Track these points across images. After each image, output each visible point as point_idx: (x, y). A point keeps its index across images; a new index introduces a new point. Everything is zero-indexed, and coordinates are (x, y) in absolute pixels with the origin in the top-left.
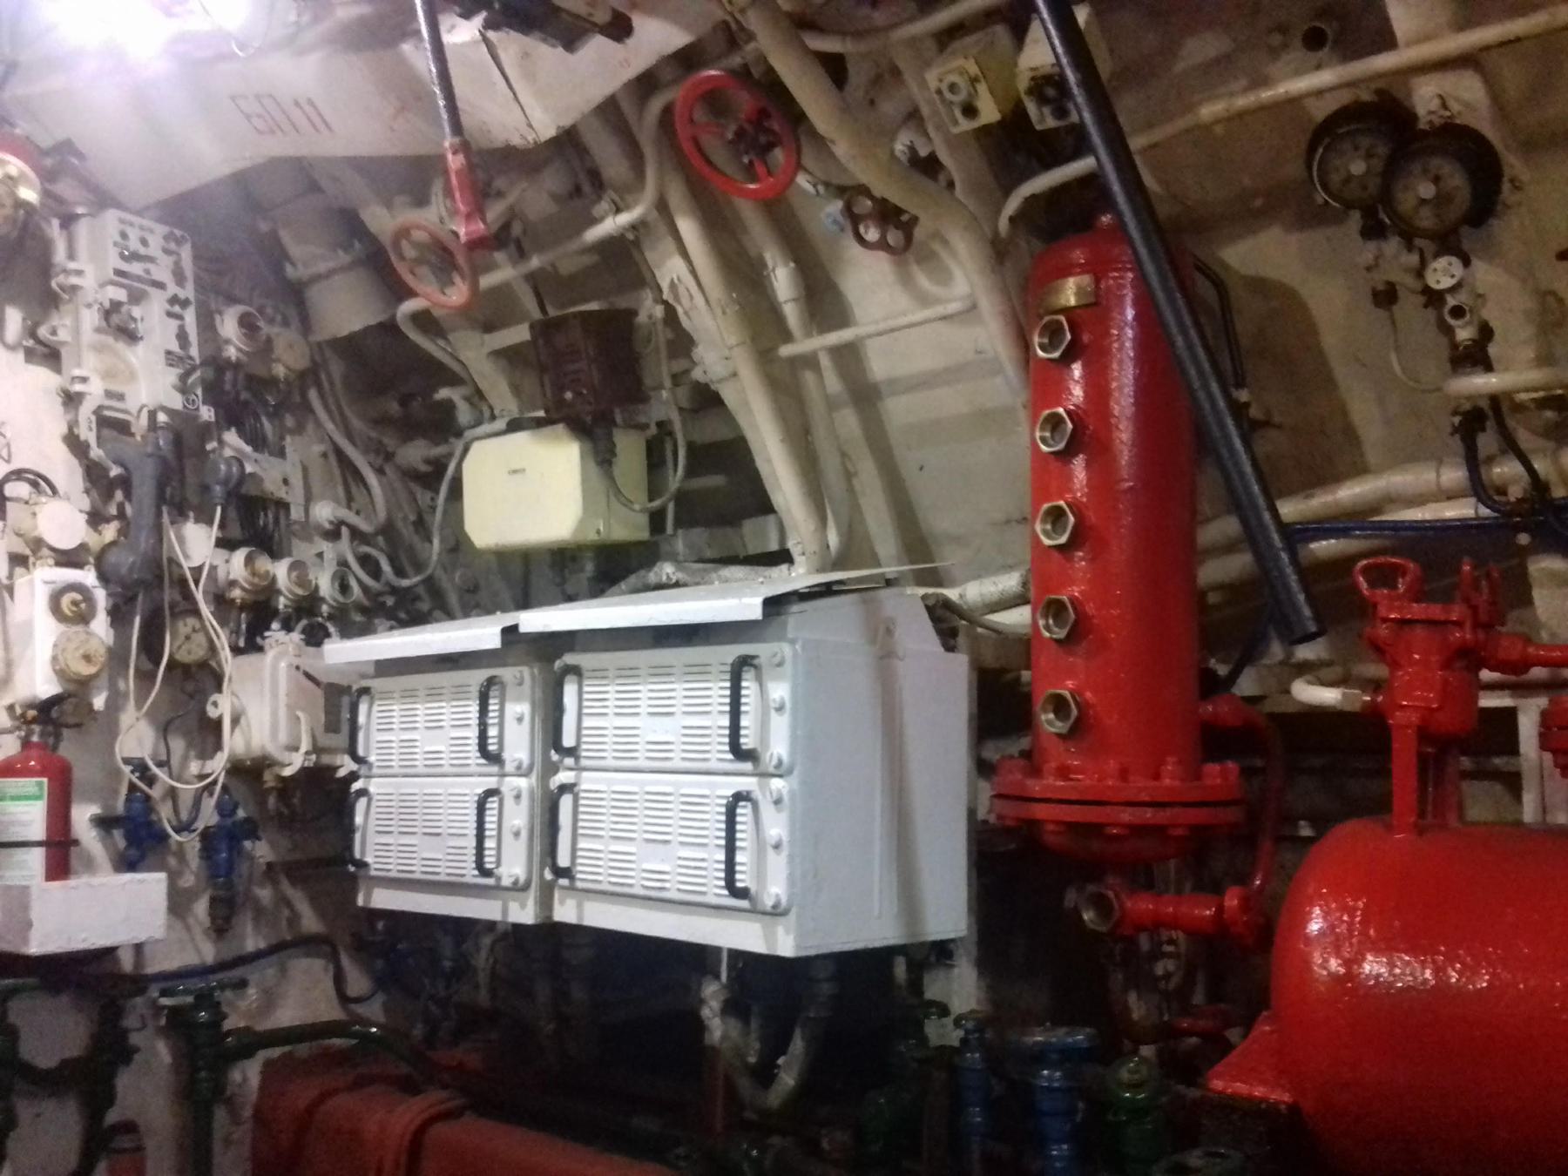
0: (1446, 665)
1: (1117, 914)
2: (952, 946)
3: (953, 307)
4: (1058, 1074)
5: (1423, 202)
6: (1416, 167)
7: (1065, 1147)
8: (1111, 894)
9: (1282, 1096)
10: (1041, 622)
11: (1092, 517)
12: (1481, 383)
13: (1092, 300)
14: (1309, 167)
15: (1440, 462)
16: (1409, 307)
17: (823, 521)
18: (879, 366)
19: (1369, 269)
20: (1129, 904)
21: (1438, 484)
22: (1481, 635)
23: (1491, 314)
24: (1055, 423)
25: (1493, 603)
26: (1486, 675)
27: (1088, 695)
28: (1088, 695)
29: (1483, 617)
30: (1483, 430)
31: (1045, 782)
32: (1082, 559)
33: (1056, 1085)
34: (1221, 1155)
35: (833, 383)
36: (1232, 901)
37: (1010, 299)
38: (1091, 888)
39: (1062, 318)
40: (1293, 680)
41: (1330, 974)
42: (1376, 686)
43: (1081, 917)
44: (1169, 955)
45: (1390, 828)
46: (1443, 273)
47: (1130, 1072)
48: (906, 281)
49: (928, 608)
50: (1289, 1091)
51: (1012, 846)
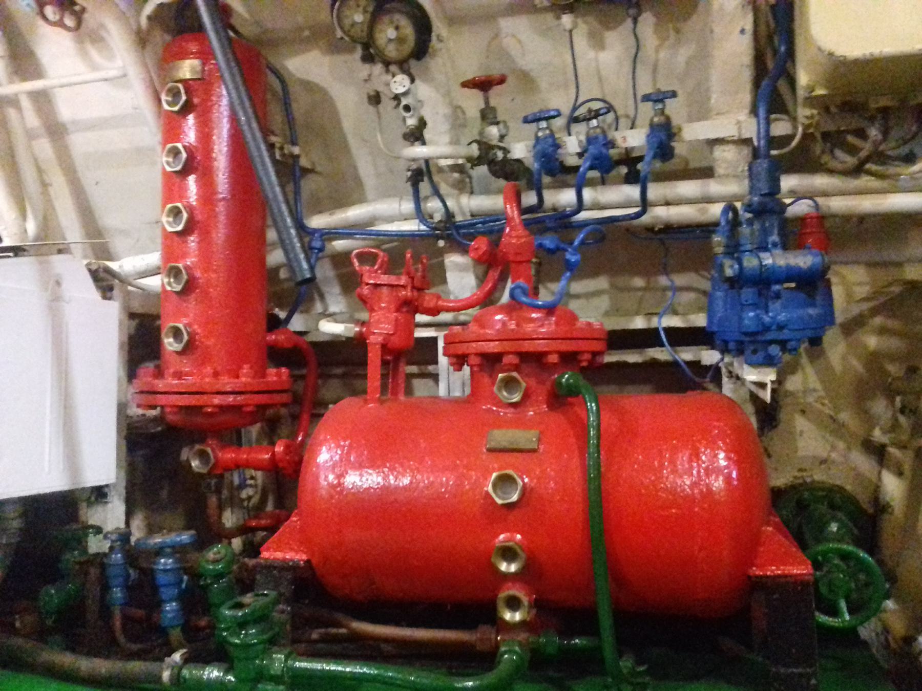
0: (398, 310)
1: (213, 460)
2: (106, 490)
3: (112, 73)
4: (171, 560)
5: (390, 40)
6: (386, 19)
7: (174, 604)
8: (209, 450)
9: (299, 557)
10: (166, 280)
11: (199, 217)
12: (419, 151)
13: (199, 76)
14: (332, 11)
15: (401, 199)
16: (387, 104)
17: (24, 216)
18: (66, 111)
19: (366, 81)
20: (220, 454)
21: (400, 210)
22: (416, 293)
23: (426, 113)
24: (175, 153)
25: (424, 277)
26: (420, 318)
27: (196, 327)
28: (196, 327)
29: (417, 283)
30: (422, 181)
31: (166, 381)
32: (193, 241)
33: (169, 567)
34: (266, 595)
35: (32, 120)
36: (279, 448)
37: (148, 72)
38: (197, 447)
39: (180, 86)
40: (322, 319)
41: (329, 484)
42: (363, 324)
43: (190, 466)
44: (251, 486)
45: (366, 402)
46: (400, 83)
47: (215, 554)
48: (84, 54)
49: (90, 270)
50: (305, 553)
51: (159, 429)
